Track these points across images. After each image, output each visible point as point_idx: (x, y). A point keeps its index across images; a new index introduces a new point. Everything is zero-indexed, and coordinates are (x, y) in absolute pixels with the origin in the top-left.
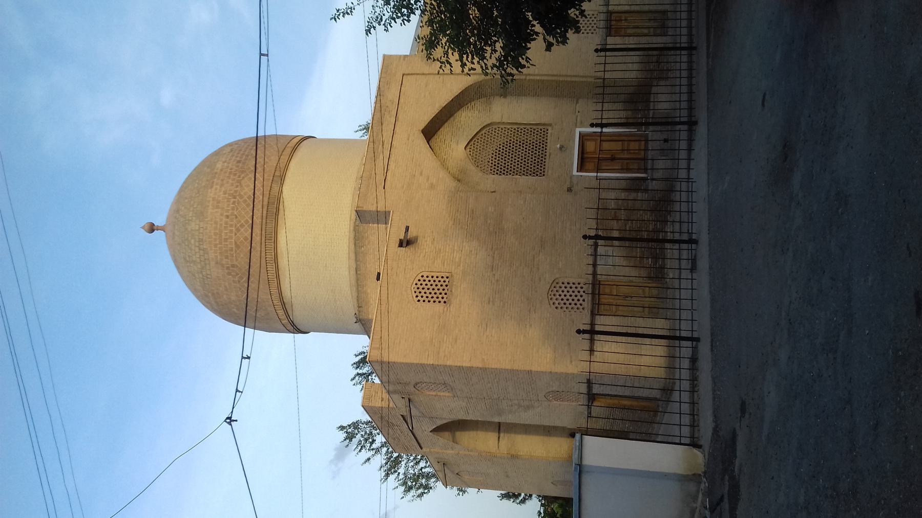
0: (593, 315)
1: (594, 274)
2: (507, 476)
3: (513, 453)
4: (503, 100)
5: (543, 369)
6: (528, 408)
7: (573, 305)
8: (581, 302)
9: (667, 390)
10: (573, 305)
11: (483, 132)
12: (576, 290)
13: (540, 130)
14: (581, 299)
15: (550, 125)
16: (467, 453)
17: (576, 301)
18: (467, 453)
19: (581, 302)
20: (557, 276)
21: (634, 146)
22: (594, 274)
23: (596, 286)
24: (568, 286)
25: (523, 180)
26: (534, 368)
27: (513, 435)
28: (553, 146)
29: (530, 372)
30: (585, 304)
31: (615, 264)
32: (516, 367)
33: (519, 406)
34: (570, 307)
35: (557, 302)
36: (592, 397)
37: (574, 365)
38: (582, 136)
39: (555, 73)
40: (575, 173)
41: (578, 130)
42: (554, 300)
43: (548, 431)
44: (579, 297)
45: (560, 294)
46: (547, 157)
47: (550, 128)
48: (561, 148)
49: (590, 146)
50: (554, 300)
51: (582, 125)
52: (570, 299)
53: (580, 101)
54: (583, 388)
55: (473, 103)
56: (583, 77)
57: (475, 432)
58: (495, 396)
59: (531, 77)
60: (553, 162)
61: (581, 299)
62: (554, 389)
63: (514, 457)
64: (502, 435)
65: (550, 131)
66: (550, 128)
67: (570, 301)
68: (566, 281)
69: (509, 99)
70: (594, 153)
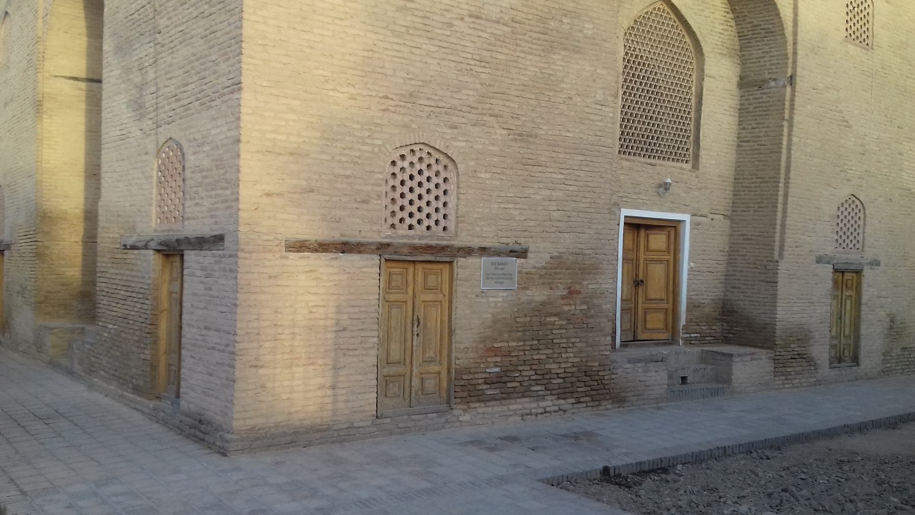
0: (381, 248)
1: (468, 251)
2: (6, 104)
3: (46, 105)
4: (735, 80)
5: (246, 119)
6: (138, 108)
7: (400, 202)
8: (408, 221)
9: (202, 432)
10: (400, 202)
11: (688, 40)
12: (431, 210)
13: (687, 148)
14: (414, 221)
15: (695, 167)
16: (41, 13)
17: (409, 209)
18: (41, 13)
19: (408, 221)
20: (461, 167)
21: (656, 320)
22: (468, 251)
23: (442, 256)
24: (440, 192)
25: (613, 113)
26: (246, 97)
27: (83, 106)
28: (668, 171)
29: (237, 86)
30: (402, 230)
31: (480, 301)
32: (248, 49)
33: (141, 87)
34: (397, 195)
35: (406, 164)
36: (172, 251)
37: (268, 199)
38: (672, 228)
39: (792, 174)
40: (625, 212)
41: (686, 217)
42: (409, 158)
43: (93, 174)
44: (418, 215)
45: (420, 175)
46: (649, 161)
47: (689, 166)
48: (666, 187)
49: (658, 241)
50: (409, 158)
51: (695, 225)
52: (414, 196)
53: (728, 222)
54: (194, 228)
55: (733, 23)
56: (783, 225)
57: (84, 30)
58: (163, 22)
59: (786, 130)
60: (642, 171)
61: (414, 221)
62: (191, 160)
63: (38, 106)
64: (83, 85)
65: (684, 165)
66: (689, 166)
67: (409, 196)
68: (451, 187)
69: (735, 90)
70: (647, 249)
